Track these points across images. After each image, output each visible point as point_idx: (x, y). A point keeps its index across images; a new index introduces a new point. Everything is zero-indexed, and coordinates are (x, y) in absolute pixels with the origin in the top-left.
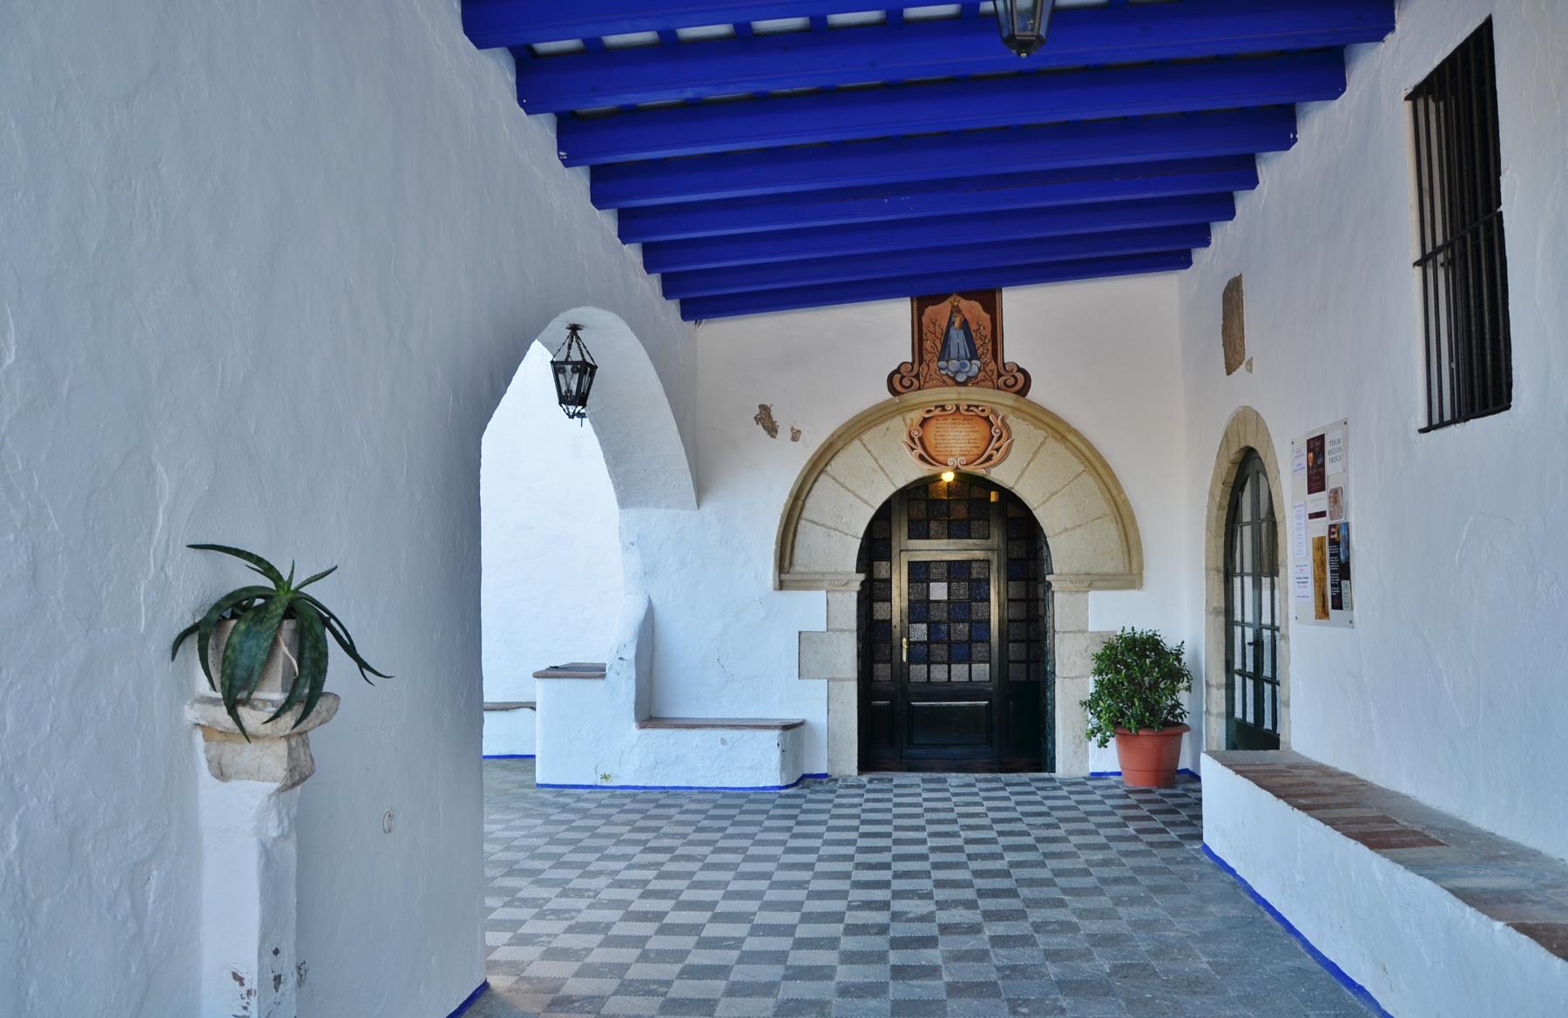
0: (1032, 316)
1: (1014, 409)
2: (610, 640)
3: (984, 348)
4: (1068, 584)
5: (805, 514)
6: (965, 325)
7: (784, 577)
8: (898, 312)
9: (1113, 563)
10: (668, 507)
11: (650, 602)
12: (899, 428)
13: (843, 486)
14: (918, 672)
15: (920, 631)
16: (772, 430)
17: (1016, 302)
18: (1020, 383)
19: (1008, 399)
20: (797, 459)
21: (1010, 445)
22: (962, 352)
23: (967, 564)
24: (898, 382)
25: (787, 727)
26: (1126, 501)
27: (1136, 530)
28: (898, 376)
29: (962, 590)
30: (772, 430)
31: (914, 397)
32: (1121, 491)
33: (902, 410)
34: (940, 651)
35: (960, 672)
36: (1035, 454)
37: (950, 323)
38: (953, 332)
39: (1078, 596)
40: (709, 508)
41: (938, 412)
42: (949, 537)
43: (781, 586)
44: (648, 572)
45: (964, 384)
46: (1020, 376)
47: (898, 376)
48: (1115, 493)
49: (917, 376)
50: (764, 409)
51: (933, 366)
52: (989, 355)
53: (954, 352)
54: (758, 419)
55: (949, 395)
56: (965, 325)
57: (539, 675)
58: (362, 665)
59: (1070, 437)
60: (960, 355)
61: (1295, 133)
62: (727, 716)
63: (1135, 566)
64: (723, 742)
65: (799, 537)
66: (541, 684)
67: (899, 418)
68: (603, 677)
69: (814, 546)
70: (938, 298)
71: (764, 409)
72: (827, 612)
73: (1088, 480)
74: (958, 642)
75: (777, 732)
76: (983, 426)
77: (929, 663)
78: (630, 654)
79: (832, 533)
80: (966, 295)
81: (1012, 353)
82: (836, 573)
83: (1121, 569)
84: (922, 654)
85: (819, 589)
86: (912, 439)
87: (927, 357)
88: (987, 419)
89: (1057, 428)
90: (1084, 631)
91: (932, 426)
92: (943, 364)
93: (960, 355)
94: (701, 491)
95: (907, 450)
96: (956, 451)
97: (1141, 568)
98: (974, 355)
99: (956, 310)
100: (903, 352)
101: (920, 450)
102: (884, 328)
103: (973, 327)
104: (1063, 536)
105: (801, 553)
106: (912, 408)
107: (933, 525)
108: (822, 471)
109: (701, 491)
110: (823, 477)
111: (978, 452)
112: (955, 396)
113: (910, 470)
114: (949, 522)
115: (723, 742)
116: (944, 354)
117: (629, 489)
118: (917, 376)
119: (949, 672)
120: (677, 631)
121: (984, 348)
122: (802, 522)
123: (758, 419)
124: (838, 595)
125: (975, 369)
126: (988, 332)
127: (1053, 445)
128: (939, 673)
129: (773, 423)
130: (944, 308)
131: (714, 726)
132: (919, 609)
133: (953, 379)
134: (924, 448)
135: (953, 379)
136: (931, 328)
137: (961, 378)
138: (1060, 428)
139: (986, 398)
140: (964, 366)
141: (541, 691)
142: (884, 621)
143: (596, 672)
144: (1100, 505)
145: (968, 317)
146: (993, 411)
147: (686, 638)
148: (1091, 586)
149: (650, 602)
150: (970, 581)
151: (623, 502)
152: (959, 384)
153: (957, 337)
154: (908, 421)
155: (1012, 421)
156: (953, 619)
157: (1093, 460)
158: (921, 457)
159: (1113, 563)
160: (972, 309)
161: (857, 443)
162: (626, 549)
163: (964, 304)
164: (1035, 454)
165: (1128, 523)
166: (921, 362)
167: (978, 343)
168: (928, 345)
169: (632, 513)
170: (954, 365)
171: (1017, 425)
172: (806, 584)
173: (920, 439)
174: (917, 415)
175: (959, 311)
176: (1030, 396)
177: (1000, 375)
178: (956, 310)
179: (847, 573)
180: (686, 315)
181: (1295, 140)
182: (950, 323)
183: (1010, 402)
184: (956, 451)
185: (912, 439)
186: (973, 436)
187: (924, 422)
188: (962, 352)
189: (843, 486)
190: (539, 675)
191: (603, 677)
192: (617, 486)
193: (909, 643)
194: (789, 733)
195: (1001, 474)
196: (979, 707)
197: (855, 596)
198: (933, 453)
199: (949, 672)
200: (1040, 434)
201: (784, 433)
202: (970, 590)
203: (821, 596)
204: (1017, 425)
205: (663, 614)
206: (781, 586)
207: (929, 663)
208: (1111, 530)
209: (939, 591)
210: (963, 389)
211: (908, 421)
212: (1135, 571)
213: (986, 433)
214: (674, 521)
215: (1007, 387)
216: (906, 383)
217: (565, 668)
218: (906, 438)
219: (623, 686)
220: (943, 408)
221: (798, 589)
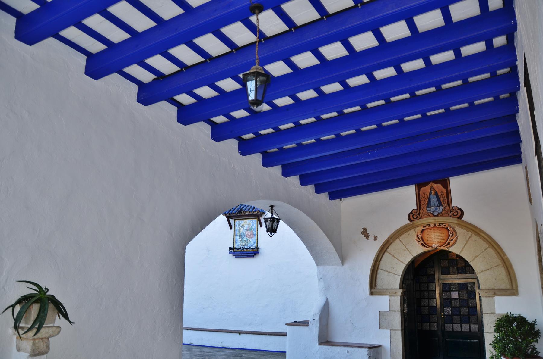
0: (461, 187)
1: (458, 225)
2: (311, 311)
3: (444, 201)
4: (484, 293)
5: (380, 267)
6: (436, 194)
7: (372, 290)
8: (410, 191)
9: (505, 285)
10: (333, 265)
11: (327, 299)
12: (413, 234)
13: (393, 256)
14: (448, 327)
15: (448, 311)
16: (367, 237)
17: (455, 182)
18: (459, 214)
19: (454, 220)
20: (376, 247)
21: (457, 238)
22: (436, 204)
23: (466, 284)
24: (412, 216)
25: (371, 347)
26: (507, 259)
27: (513, 270)
28: (412, 215)
29: (464, 295)
30: (367, 237)
31: (417, 222)
32: (505, 255)
33: (414, 227)
34: (457, 318)
35: (466, 328)
36: (467, 241)
37: (430, 193)
38: (431, 196)
39: (490, 298)
40: (346, 266)
41: (427, 227)
42: (458, 274)
43: (372, 294)
44: (327, 289)
45: (437, 216)
46: (459, 211)
47: (412, 215)
48: (502, 256)
49: (419, 214)
50: (364, 229)
51: (425, 210)
52: (446, 204)
53: (432, 204)
54: (362, 233)
55: (431, 220)
56: (436, 194)
57: (288, 324)
58: (70, 322)
59: (481, 234)
60: (437, 205)
61: (518, 106)
62: (354, 342)
63: (514, 286)
64: (348, 352)
65: (378, 275)
66: (288, 327)
67: (413, 230)
68: (308, 326)
69: (383, 279)
70: (425, 184)
71: (364, 229)
72: (390, 304)
73: (491, 251)
74: (464, 315)
75: (367, 349)
76: (446, 231)
77: (469, 323)
78: (317, 318)
79: (390, 274)
80: (436, 182)
81: (455, 202)
82: (392, 289)
83: (508, 287)
84: (450, 319)
85: (386, 295)
86: (418, 238)
87: (422, 207)
88: (447, 228)
89: (476, 231)
90: (493, 313)
91: (425, 232)
92: (428, 209)
93: (437, 205)
94: (343, 259)
95: (417, 242)
96: (436, 241)
97: (517, 287)
98: (440, 204)
99: (432, 188)
100: (413, 205)
101: (421, 242)
102: (406, 196)
103: (439, 194)
104: (481, 274)
105: (379, 282)
106: (418, 226)
107: (451, 269)
108: (385, 251)
109: (343, 259)
110: (386, 253)
111: (444, 241)
112: (433, 221)
113: (418, 249)
114: (458, 268)
115: (348, 352)
116: (429, 205)
117: (319, 259)
118: (419, 214)
119: (470, 327)
120: (336, 310)
121: (444, 201)
122: (379, 270)
123: (362, 233)
124: (393, 297)
125: (441, 210)
126: (445, 195)
127: (474, 237)
128: (457, 327)
129: (368, 234)
130: (428, 188)
131: (344, 346)
132: (446, 302)
133: (433, 214)
134: (423, 241)
135: (433, 214)
136: (423, 195)
137: (436, 214)
138: (477, 231)
139: (445, 221)
140: (437, 209)
141: (287, 330)
142: (434, 306)
143: (305, 323)
144: (497, 260)
145: (437, 190)
146: (449, 226)
147: (339, 312)
148: (495, 294)
149: (327, 299)
150: (468, 291)
151: (318, 264)
152: (435, 216)
153: (433, 198)
154: (417, 231)
155: (458, 229)
156: (461, 306)
157: (492, 243)
158: (422, 244)
159: (505, 285)
160: (438, 187)
161: (398, 240)
162: (319, 280)
163: (435, 186)
164: (467, 241)
165: (509, 268)
166: (420, 209)
167: (442, 200)
168: (422, 202)
169: (321, 267)
170: (433, 209)
171: (459, 230)
172: (381, 293)
173: (421, 238)
174: (420, 229)
175: (434, 189)
176: (463, 219)
177: (451, 211)
178: (432, 188)
179: (396, 289)
180: (332, 197)
181: (518, 108)
182: (430, 193)
183: (456, 222)
184: (436, 241)
185: (418, 238)
186: (442, 235)
187: (423, 231)
188: (436, 204)
189: (393, 256)
190: (288, 324)
191: (308, 326)
192: (314, 258)
193: (444, 315)
194: (372, 350)
195: (455, 249)
196: (474, 342)
197: (399, 298)
198: (427, 243)
199: (470, 327)
200: (469, 233)
201: (371, 238)
202: (467, 294)
203: (387, 297)
204: (459, 230)
205: (332, 304)
206: (372, 294)
207: (453, 323)
208: (502, 272)
209: (455, 295)
210: (436, 218)
211: (417, 231)
212: (514, 288)
213: (447, 234)
214: (334, 269)
215: (454, 216)
216: (415, 217)
217: (299, 322)
218: (416, 237)
219: (314, 330)
220: (430, 225)
221: (379, 295)
